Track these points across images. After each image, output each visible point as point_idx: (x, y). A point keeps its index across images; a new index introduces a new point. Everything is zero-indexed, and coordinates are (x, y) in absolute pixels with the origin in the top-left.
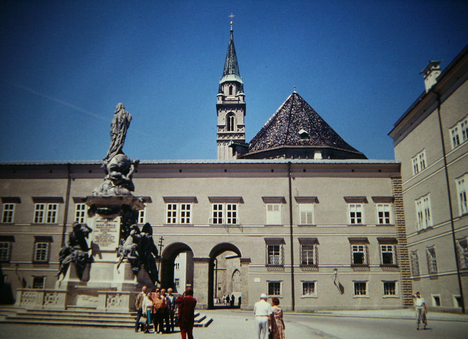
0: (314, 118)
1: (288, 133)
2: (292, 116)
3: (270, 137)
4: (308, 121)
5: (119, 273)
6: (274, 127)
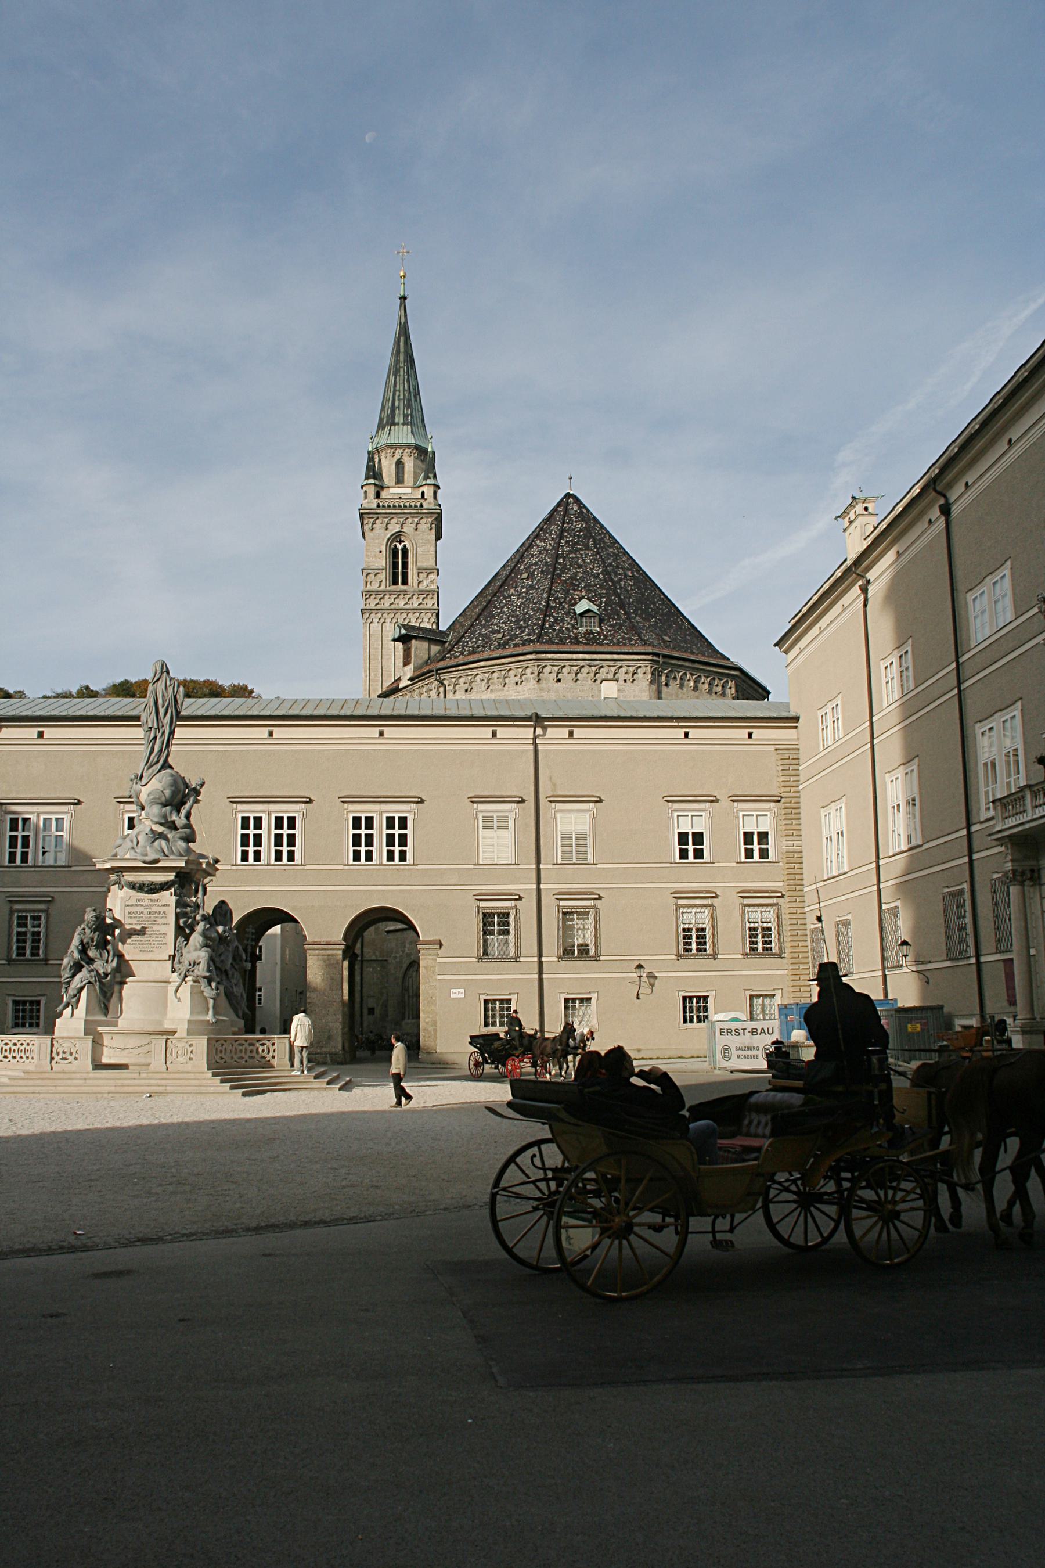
0: (618, 567)
1: (547, 611)
2: (561, 560)
3: (501, 618)
4: (601, 576)
5: (179, 1000)
6: (512, 591)
